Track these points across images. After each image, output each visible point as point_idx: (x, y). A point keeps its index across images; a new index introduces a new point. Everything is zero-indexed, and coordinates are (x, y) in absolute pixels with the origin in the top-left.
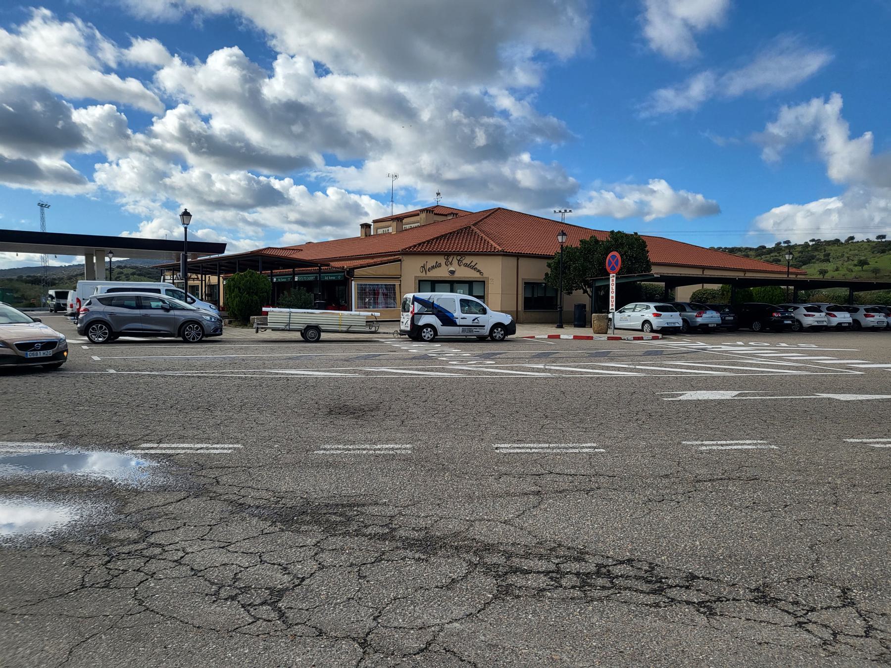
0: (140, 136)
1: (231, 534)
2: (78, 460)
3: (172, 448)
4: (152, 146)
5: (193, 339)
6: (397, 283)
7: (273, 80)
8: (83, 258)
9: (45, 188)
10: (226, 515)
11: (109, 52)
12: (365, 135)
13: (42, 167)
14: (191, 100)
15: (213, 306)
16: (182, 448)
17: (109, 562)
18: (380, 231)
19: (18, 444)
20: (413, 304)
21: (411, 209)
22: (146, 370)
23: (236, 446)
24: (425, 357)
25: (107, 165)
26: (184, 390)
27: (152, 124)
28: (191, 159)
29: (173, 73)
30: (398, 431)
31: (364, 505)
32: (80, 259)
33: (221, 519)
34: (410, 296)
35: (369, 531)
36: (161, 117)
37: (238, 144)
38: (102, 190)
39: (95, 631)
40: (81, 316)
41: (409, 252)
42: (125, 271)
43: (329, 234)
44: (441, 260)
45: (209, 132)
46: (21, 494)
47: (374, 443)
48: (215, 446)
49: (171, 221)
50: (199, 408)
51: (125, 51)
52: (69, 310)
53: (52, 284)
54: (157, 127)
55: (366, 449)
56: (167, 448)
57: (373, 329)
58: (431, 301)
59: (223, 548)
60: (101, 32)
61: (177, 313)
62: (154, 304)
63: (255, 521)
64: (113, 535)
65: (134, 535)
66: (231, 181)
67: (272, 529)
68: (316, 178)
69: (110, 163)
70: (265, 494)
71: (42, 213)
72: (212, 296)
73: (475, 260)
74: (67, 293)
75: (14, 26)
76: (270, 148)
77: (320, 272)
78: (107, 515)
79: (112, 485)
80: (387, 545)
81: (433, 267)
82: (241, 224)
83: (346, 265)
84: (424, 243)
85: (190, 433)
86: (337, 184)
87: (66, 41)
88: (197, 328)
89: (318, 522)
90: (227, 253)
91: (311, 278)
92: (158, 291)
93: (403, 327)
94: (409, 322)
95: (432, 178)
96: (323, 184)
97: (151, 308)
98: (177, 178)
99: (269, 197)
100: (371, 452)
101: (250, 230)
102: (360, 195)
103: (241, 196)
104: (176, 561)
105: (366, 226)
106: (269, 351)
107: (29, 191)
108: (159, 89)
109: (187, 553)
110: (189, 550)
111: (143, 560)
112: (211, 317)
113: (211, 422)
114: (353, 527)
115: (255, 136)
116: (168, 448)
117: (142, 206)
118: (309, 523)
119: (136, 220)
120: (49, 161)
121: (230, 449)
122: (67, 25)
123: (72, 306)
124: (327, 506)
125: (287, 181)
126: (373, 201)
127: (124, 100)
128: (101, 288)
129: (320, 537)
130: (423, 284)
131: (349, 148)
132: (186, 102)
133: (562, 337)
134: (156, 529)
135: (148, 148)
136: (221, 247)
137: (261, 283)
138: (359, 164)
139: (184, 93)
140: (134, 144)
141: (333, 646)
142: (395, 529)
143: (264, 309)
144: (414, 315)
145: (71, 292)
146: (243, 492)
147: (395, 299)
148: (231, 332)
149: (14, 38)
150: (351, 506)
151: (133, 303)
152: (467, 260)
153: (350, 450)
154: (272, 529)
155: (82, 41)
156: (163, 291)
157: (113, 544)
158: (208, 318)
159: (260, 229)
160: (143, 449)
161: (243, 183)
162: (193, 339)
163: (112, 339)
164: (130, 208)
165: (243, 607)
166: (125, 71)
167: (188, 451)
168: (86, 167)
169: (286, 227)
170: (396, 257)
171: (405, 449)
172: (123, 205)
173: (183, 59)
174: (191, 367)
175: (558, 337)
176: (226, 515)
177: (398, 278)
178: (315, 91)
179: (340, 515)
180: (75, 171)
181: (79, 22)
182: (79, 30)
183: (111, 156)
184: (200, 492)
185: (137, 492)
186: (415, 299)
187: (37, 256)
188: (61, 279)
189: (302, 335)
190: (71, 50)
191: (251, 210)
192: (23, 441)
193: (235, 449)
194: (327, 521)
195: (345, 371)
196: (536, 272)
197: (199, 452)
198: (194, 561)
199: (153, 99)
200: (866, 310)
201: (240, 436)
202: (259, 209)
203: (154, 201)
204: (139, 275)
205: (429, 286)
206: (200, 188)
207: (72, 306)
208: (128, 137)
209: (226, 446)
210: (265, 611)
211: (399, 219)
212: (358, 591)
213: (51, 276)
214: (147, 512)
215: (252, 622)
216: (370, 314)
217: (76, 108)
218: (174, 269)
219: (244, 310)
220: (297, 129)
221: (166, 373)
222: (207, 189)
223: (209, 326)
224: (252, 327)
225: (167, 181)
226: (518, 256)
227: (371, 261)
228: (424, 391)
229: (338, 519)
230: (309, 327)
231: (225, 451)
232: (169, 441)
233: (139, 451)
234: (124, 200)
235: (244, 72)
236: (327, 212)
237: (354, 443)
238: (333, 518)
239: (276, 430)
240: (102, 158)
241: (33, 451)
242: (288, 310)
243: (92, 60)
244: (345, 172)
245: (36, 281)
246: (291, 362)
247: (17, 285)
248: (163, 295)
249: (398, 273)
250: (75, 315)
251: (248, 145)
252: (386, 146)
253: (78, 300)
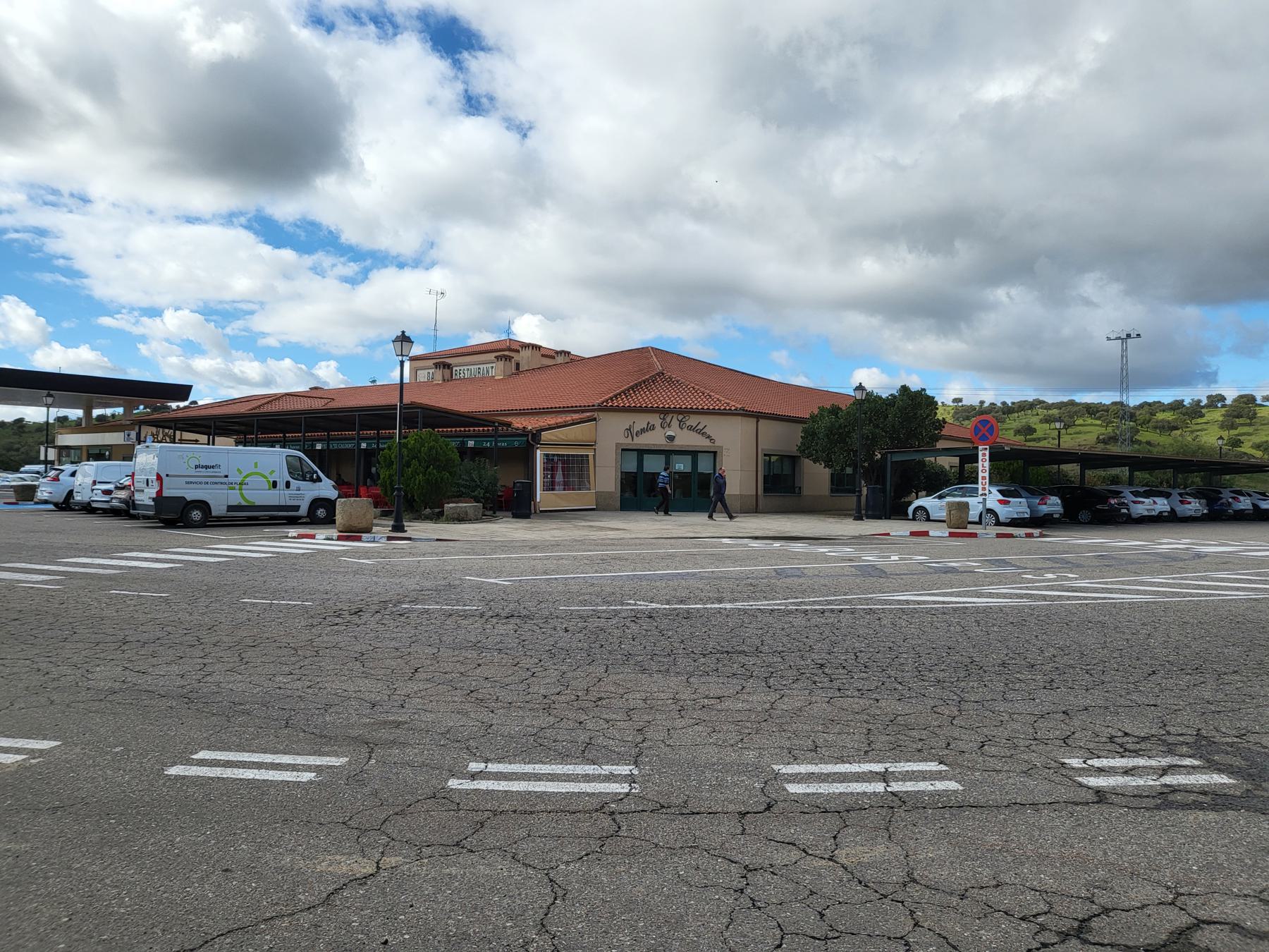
2: (901, 559)
44: (655, 419)
73: (704, 421)
81: (643, 431)
83: (531, 424)
133: (931, 533)
136: (182, 391)
152: (693, 420)
170: (589, 414)
175: (926, 534)
177: (591, 445)
196: (778, 438)
200: (1181, 495)
226: (759, 416)
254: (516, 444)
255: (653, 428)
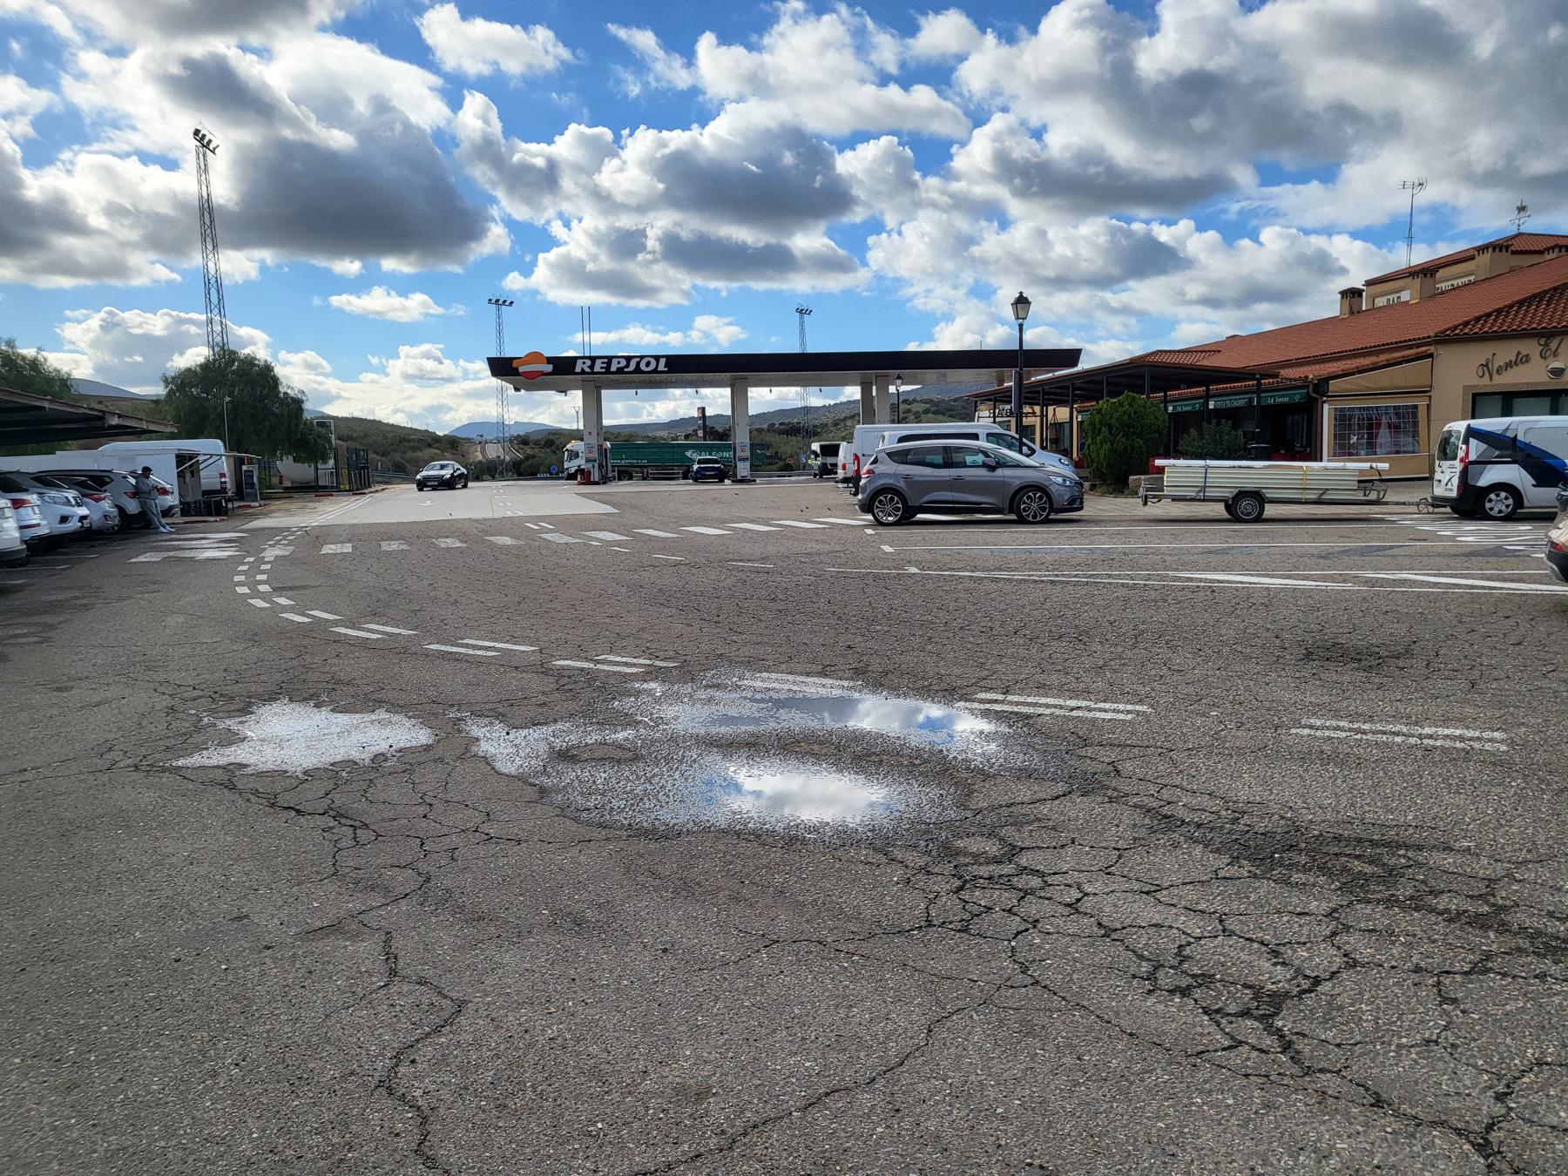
0: (933, 181)
1: (1158, 871)
2: (842, 706)
3: (1029, 704)
4: (952, 196)
5: (1035, 517)
6: (1422, 403)
7: (1158, 37)
8: (858, 389)
9: (801, 284)
10: (1143, 833)
11: (887, 49)
12: (1344, 112)
13: (797, 253)
14: (1013, 106)
15: (1065, 460)
16: (1046, 705)
17: (961, 888)
18: (1380, 302)
19: (802, 678)
20: (1466, 442)
21: (1444, 250)
22: (964, 569)
23: (1138, 708)
24: (1498, 552)
25: (884, 235)
26: (1031, 604)
27: (950, 157)
28: (1015, 207)
29: (983, 65)
30: (1466, 701)
31: (1420, 848)
32: (853, 393)
33: (1135, 839)
34: (1460, 426)
35: (1443, 902)
36: (963, 144)
37: (1092, 170)
38: (879, 277)
39: (960, 1004)
40: (863, 482)
41: (1448, 338)
42: (914, 408)
43: (1264, 318)
44: (1532, 347)
45: (1044, 156)
46: (818, 757)
47: (1416, 724)
48: (1102, 705)
49: (983, 318)
50: (1058, 638)
51: (911, 42)
52: (841, 474)
53: (813, 433)
54: (959, 162)
55: (1399, 733)
56: (1018, 702)
57: (1373, 496)
58: (1510, 434)
59: (1147, 893)
60: (874, 18)
61: (1007, 472)
62: (969, 459)
63: (1198, 850)
64: (960, 844)
65: (993, 848)
66: (1083, 237)
67: (1233, 871)
68: (1240, 212)
69: (889, 233)
70: (1206, 802)
71: (802, 324)
72: (1056, 441)
74: (837, 447)
75: (754, 38)
76: (1150, 167)
77: (1259, 390)
78: (944, 809)
79: (945, 758)
80: (1492, 941)
81: (1509, 365)
82: (1099, 314)
83: (1312, 372)
84: (1489, 315)
85: (1054, 679)
86: (1282, 220)
87: (827, 45)
88: (1040, 498)
89: (1323, 869)
90: (1084, 365)
91: (1240, 402)
92: (975, 437)
93: (1439, 491)
94: (1456, 481)
95: (1489, 179)
96: (1255, 222)
97: (964, 465)
98: (992, 243)
99: (1151, 259)
100: (1412, 741)
101: (1116, 323)
102: (1330, 235)
103: (1100, 263)
104: (1067, 905)
105: (1352, 294)
106: (1164, 536)
107: (781, 292)
108: (960, 95)
109: (1087, 894)
110: (1088, 889)
111: (1015, 895)
112: (1065, 478)
113: (1088, 663)
114: (1404, 891)
115: (1123, 150)
116: (1022, 704)
117: (935, 297)
118: (1306, 869)
119: (930, 321)
120: (808, 240)
121: (1129, 712)
122: (826, 18)
123: (844, 467)
124: (1338, 839)
125: (1185, 225)
126: (1358, 244)
127: (907, 126)
128: (888, 436)
129: (1336, 900)
130: (1478, 403)
131: (1302, 142)
132: (1005, 110)
134: (1027, 844)
135: (946, 199)
136: (1072, 356)
137: (1141, 417)
138: (1328, 174)
139: (1000, 94)
140: (924, 195)
141: (1413, 1135)
142: (1503, 908)
143: (1158, 462)
144: (1467, 466)
145: (843, 445)
146: (1165, 794)
147: (1415, 434)
148: (1097, 505)
149: (755, 56)
150: (1394, 846)
151: (939, 459)
153: (1364, 732)
154: (1233, 871)
155: (848, 39)
156: (982, 436)
157: (961, 859)
158: (1060, 480)
159: (1133, 321)
160: (982, 701)
161: (1102, 240)
162: (1035, 517)
163: (906, 519)
164: (919, 303)
165: (1205, 1013)
166: (908, 77)
167: (1057, 712)
168: (856, 242)
169: (1182, 311)
170: (1421, 349)
171: (1491, 740)
172: (909, 300)
173: (1000, 36)
174: (1036, 565)
176: (1143, 833)
177: (1424, 392)
178: (1238, 41)
179: (1371, 862)
180: (841, 251)
181: (843, 9)
182: (844, 23)
183: (890, 221)
184: (1088, 786)
185: (986, 776)
186: (1471, 433)
187: (792, 391)
188: (824, 426)
189: (1228, 507)
190: (832, 58)
191: (1117, 287)
192: (808, 674)
193: (1138, 713)
194: (1345, 869)
195: (1324, 578)
197: (1074, 713)
198: (1101, 910)
199: (954, 114)
201: (1143, 691)
202: (1132, 283)
203: (955, 288)
204: (935, 413)
205: (1497, 403)
206: (1028, 256)
207: (844, 467)
208: (914, 185)
209: (1121, 707)
210: (1249, 1028)
211: (1427, 272)
212: (1446, 1028)
213: (813, 421)
214: (1005, 811)
215: (1230, 1048)
216: (1367, 465)
217: (841, 151)
218: (997, 398)
219: (1118, 464)
220: (1201, 123)
221: (997, 574)
222: (1040, 257)
223: (1060, 493)
224: (1135, 493)
225: (976, 250)
227: (1368, 361)
228: (1512, 622)
229: (1368, 869)
230: (1242, 494)
231: (1121, 716)
232: (1022, 692)
233: (976, 705)
234: (911, 291)
235: (1103, 34)
236: (1261, 277)
237: (1371, 719)
238: (1357, 866)
239: (1208, 685)
240: (876, 226)
241: (824, 692)
242: (1202, 463)
243: (862, 67)
244: (1297, 194)
245: (792, 430)
246: (1213, 558)
247: (768, 438)
248: (982, 443)
249: (1426, 381)
250: (853, 481)
251: (1111, 170)
252: (1388, 126)
253: (856, 457)
254: (1297, 398)
255: (1527, 359)
